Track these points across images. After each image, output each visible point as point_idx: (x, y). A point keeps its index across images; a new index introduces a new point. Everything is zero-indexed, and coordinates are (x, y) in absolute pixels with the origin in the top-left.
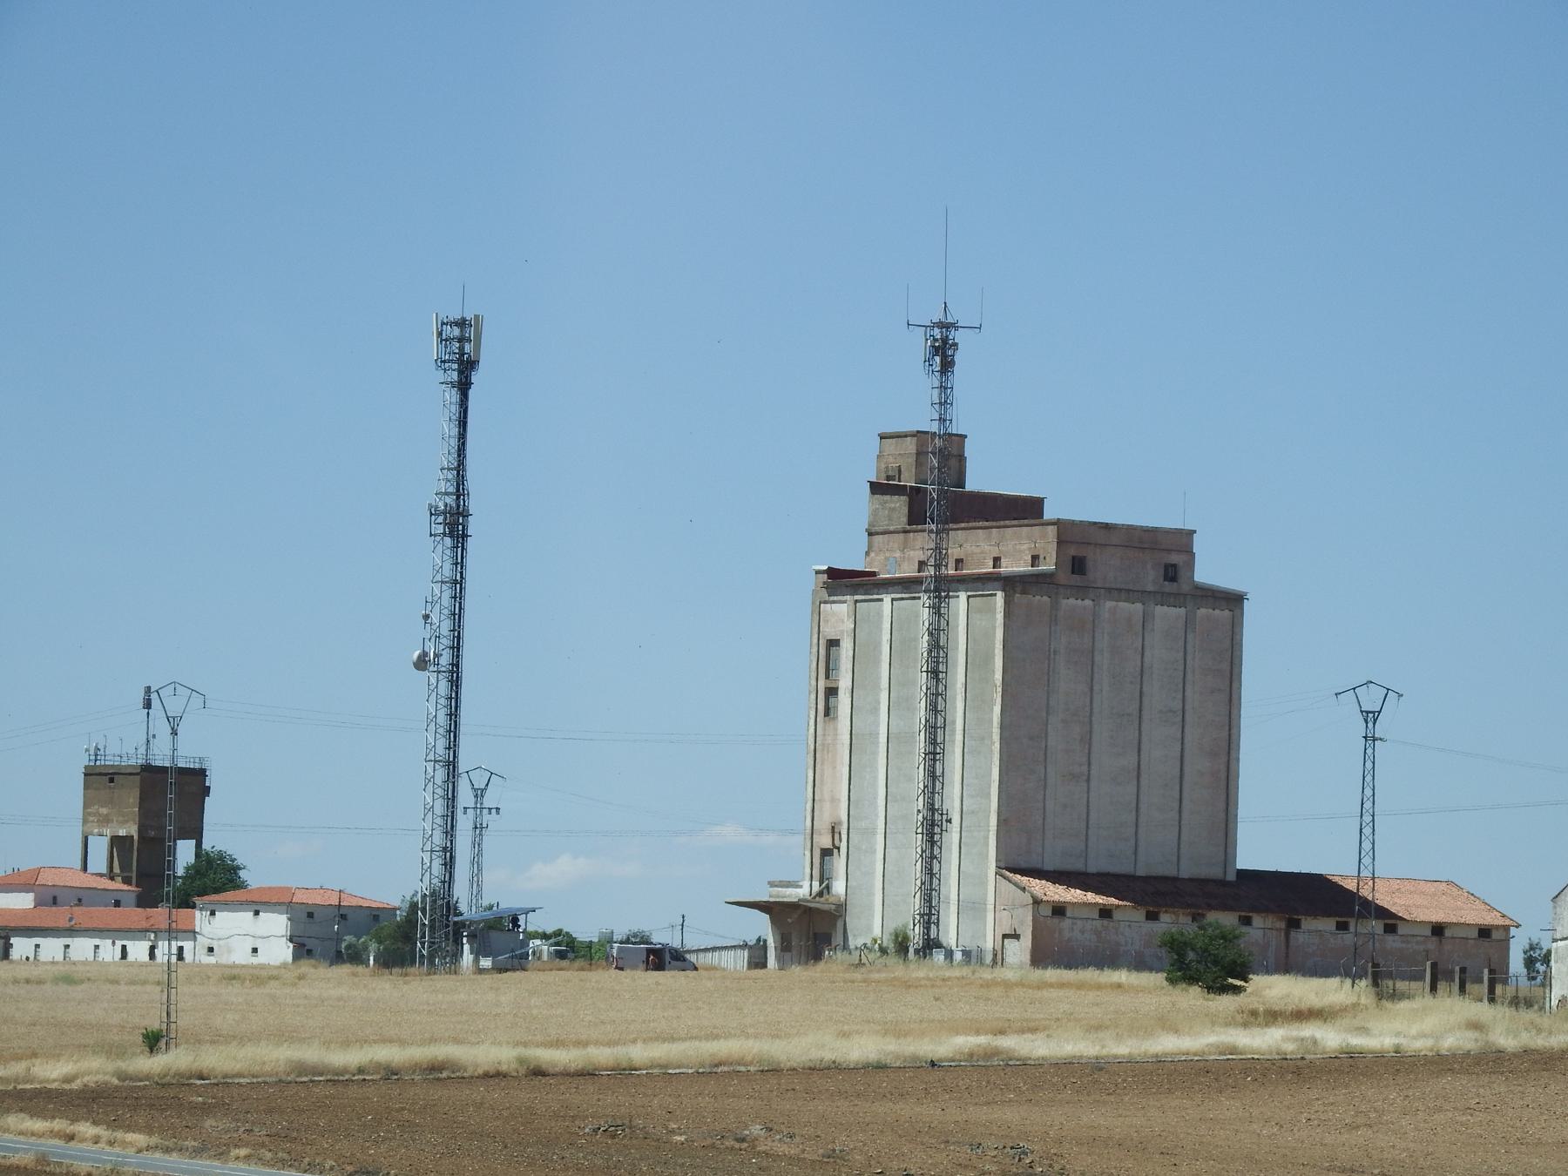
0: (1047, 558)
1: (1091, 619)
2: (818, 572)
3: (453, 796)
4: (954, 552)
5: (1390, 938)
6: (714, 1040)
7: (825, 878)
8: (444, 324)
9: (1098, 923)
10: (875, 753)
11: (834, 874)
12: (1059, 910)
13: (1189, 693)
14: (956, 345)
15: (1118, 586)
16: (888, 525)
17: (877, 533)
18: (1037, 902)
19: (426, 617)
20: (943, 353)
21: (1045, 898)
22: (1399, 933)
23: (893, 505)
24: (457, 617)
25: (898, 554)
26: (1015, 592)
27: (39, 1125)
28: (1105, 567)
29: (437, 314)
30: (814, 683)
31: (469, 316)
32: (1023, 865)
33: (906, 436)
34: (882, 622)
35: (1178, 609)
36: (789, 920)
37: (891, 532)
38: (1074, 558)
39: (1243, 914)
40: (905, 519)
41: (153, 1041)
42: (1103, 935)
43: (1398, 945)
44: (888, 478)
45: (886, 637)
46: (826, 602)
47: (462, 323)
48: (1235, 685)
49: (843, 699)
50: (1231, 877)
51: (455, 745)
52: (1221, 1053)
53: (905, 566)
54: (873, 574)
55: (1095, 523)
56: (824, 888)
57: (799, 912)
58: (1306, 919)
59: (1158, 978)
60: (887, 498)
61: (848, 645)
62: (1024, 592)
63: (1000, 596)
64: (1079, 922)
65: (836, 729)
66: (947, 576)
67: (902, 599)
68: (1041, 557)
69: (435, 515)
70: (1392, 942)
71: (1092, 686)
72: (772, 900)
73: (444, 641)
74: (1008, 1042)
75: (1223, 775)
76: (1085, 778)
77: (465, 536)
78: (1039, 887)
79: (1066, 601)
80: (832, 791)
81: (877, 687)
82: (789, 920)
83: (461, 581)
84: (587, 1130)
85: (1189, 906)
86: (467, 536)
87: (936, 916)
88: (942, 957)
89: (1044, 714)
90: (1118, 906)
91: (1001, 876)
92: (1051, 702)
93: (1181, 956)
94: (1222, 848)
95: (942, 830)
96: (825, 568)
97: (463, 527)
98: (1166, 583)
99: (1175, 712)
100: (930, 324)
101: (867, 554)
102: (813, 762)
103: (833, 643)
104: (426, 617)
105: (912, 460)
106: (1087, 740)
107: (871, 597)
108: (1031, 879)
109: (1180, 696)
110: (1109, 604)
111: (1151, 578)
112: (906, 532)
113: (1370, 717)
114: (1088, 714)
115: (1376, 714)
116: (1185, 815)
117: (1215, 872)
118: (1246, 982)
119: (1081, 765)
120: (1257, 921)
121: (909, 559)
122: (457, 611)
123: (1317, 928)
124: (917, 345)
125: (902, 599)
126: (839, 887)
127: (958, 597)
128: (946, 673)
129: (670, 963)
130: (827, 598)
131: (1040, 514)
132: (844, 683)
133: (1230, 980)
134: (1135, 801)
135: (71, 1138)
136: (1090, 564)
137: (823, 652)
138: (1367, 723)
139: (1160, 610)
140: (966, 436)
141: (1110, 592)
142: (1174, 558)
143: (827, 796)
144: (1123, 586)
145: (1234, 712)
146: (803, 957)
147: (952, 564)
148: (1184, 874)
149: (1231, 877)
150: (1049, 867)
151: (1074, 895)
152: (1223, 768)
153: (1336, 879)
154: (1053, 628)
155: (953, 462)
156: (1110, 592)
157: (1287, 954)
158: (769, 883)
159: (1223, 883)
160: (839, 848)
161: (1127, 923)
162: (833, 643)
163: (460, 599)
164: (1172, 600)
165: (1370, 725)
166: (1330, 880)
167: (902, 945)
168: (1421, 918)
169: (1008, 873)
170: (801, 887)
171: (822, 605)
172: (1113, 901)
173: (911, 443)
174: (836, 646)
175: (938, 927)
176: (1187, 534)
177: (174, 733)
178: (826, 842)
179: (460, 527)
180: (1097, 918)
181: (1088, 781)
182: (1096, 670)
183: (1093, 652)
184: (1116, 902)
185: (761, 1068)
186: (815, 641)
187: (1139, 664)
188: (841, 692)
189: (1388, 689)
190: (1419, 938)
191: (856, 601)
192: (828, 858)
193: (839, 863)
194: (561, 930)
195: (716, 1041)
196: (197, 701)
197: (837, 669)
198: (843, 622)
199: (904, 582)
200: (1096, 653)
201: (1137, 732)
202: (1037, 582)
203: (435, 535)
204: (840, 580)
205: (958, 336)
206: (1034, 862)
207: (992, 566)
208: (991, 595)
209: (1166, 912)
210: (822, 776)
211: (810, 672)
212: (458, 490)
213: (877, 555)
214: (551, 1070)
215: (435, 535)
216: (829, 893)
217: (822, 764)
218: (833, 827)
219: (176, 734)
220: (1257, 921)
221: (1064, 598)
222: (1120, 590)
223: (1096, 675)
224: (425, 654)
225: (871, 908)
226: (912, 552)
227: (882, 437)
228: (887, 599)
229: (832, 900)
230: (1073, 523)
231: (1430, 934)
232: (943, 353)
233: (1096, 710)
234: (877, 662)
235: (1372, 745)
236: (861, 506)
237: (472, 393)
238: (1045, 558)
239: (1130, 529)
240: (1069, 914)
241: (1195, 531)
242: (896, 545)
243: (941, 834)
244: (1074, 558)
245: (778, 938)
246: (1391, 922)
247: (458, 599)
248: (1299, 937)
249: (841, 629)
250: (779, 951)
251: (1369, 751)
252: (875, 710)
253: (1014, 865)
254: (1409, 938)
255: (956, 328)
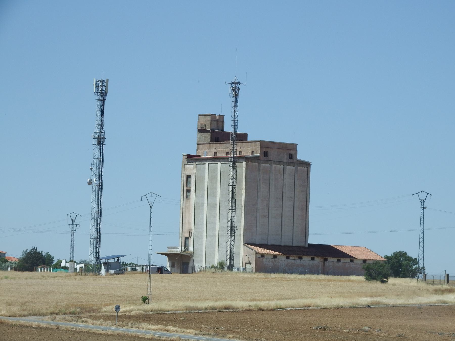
0: (257, 152)
1: (269, 170)
2: (183, 155)
3: (100, 222)
4: (239, 150)
5: (351, 263)
6: (314, 299)
7: (186, 246)
8: (97, 81)
9: (273, 260)
10: (203, 209)
11: (189, 245)
12: (263, 256)
13: (295, 192)
14: (239, 89)
15: (277, 160)
16: (204, 142)
17: (200, 144)
18: (257, 253)
19: (91, 169)
20: (235, 92)
21: (259, 252)
22: (265, 257)
23: (205, 136)
24: (101, 169)
25: (207, 150)
26: (249, 162)
27: (155, 327)
28: (273, 154)
29: (95, 79)
30: (183, 188)
31: (105, 79)
32: (250, 242)
33: (207, 115)
34: (205, 171)
35: (293, 167)
36: (177, 258)
37: (205, 144)
38: (264, 152)
39: (312, 257)
40: (209, 140)
41: (145, 300)
42: (274, 263)
43: (354, 266)
44: (202, 128)
45: (207, 175)
46: (186, 164)
47: (102, 81)
48: (308, 190)
49: (192, 194)
50: (307, 246)
51: (101, 207)
52: (442, 303)
53: (210, 154)
54: (199, 156)
55: (270, 142)
56: (185, 249)
57: (179, 256)
58: (329, 258)
59: (362, 278)
60: (203, 134)
61: (194, 177)
62: (251, 162)
63: (244, 163)
64: (268, 259)
65: (190, 202)
66: (237, 156)
67: (212, 164)
68: (255, 152)
69: (95, 138)
70: (352, 265)
71: (269, 190)
72: (169, 252)
73: (97, 176)
74: (379, 299)
75: (305, 216)
76: (268, 217)
77: (103, 145)
78: (257, 249)
79: (262, 164)
80: (188, 220)
81: (204, 190)
82: (177, 258)
83: (102, 158)
84: (314, 328)
85: (298, 255)
86: (104, 145)
87: (233, 258)
88: (236, 270)
89: (256, 198)
90: (279, 255)
91: (245, 245)
92: (258, 195)
93: (369, 271)
94: (304, 238)
95: (235, 232)
96: (186, 154)
97: (103, 142)
98: (290, 159)
99: (292, 197)
100: (231, 83)
101: (197, 150)
102: (182, 212)
103: (189, 177)
104: (91, 169)
105: (209, 123)
106: (268, 205)
107: (201, 163)
108: (254, 247)
109: (293, 193)
110: (274, 165)
111: (285, 158)
112: (210, 144)
113: (423, 201)
114: (268, 198)
115: (424, 201)
116: (295, 227)
117: (302, 244)
118: (387, 279)
119: (266, 213)
120: (291, 258)
121: (211, 152)
122: (101, 167)
123: (332, 260)
124: (228, 89)
125: (212, 164)
126: (191, 249)
127: (243, 162)
128: (236, 186)
129: (164, 272)
130: (187, 164)
131: (246, 139)
132: (192, 188)
133: (383, 279)
134: (281, 224)
135: (168, 331)
136: (269, 154)
137: (185, 179)
138: (421, 203)
139: (288, 167)
140: (224, 116)
141: (274, 162)
142: (292, 152)
143: (187, 221)
144: (278, 160)
145: (308, 197)
146: (179, 269)
147: (238, 153)
148: (294, 245)
149: (307, 246)
150: (258, 243)
151: (267, 251)
152: (305, 214)
153: (334, 246)
154: (259, 172)
155: (221, 123)
156: (274, 162)
157: (324, 268)
158: (167, 247)
159: (305, 247)
160: (191, 237)
161: (281, 260)
162: (189, 177)
163: (102, 163)
164: (291, 164)
165: (422, 204)
166: (333, 247)
167: (221, 265)
168: (360, 258)
169: (250, 246)
170: (178, 248)
171: (185, 165)
172: (277, 253)
173: (209, 117)
174: (190, 178)
175: (234, 261)
176: (295, 145)
177: (151, 208)
178: (187, 235)
179: (102, 142)
180: (285, 258)
181: (268, 218)
182: (270, 185)
183: (270, 179)
184: (278, 253)
185: (322, 308)
186: (183, 176)
187: (282, 183)
188: (191, 191)
189: (428, 193)
190: (359, 264)
191: (196, 164)
192: (187, 240)
193: (191, 242)
194: (131, 263)
195: (314, 299)
196: (159, 198)
197: (190, 184)
198: (192, 170)
199: (213, 159)
200: (271, 180)
201: (282, 203)
202: (255, 159)
203: (94, 144)
204: (190, 158)
205: (240, 86)
206: (253, 241)
207: (238, 154)
208: (242, 163)
209: (292, 256)
210: (185, 216)
211: (181, 185)
212: (101, 131)
213: (200, 150)
214: (264, 309)
215: (94, 144)
216: (187, 251)
217: (185, 211)
218: (189, 231)
219: (152, 208)
220: (316, 259)
221: (262, 164)
222: (277, 161)
223: (270, 188)
224: (91, 180)
225: (202, 256)
226: (212, 150)
227: (199, 116)
228: (207, 164)
229: (189, 252)
230: (264, 141)
231: (362, 262)
232: (235, 92)
233: (270, 196)
234: (204, 182)
235: (423, 210)
236: (195, 136)
237: (106, 102)
238: (256, 152)
239: (280, 143)
240: (265, 257)
241: (297, 144)
242: (207, 148)
243: (234, 233)
244: (264, 152)
245: (171, 264)
246: (352, 259)
247: (101, 164)
248: (327, 263)
249: (191, 172)
250: (171, 267)
251: (422, 212)
252: (203, 196)
253: (248, 243)
254: (357, 264)
255: (239, 84)
